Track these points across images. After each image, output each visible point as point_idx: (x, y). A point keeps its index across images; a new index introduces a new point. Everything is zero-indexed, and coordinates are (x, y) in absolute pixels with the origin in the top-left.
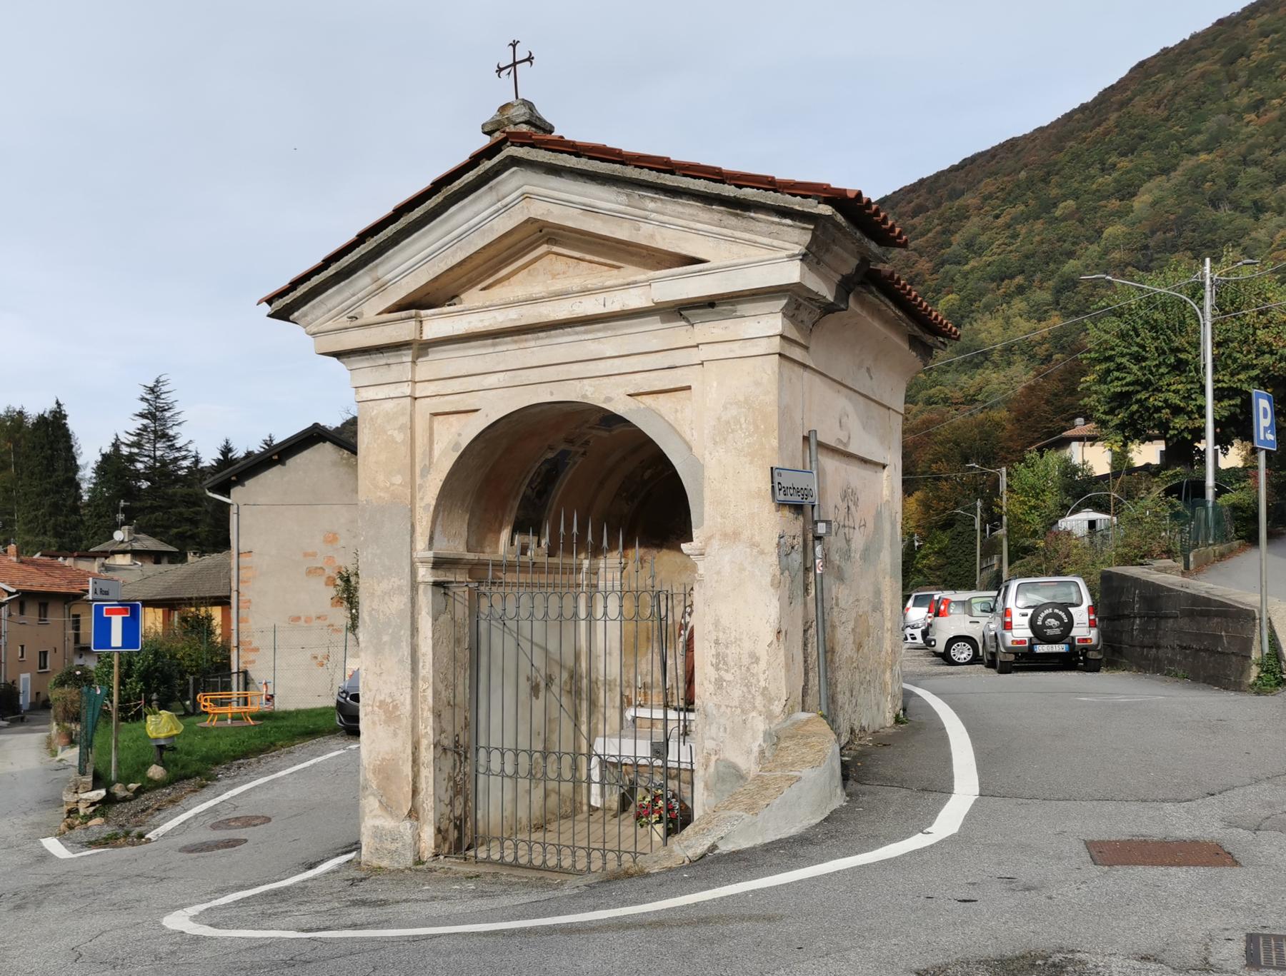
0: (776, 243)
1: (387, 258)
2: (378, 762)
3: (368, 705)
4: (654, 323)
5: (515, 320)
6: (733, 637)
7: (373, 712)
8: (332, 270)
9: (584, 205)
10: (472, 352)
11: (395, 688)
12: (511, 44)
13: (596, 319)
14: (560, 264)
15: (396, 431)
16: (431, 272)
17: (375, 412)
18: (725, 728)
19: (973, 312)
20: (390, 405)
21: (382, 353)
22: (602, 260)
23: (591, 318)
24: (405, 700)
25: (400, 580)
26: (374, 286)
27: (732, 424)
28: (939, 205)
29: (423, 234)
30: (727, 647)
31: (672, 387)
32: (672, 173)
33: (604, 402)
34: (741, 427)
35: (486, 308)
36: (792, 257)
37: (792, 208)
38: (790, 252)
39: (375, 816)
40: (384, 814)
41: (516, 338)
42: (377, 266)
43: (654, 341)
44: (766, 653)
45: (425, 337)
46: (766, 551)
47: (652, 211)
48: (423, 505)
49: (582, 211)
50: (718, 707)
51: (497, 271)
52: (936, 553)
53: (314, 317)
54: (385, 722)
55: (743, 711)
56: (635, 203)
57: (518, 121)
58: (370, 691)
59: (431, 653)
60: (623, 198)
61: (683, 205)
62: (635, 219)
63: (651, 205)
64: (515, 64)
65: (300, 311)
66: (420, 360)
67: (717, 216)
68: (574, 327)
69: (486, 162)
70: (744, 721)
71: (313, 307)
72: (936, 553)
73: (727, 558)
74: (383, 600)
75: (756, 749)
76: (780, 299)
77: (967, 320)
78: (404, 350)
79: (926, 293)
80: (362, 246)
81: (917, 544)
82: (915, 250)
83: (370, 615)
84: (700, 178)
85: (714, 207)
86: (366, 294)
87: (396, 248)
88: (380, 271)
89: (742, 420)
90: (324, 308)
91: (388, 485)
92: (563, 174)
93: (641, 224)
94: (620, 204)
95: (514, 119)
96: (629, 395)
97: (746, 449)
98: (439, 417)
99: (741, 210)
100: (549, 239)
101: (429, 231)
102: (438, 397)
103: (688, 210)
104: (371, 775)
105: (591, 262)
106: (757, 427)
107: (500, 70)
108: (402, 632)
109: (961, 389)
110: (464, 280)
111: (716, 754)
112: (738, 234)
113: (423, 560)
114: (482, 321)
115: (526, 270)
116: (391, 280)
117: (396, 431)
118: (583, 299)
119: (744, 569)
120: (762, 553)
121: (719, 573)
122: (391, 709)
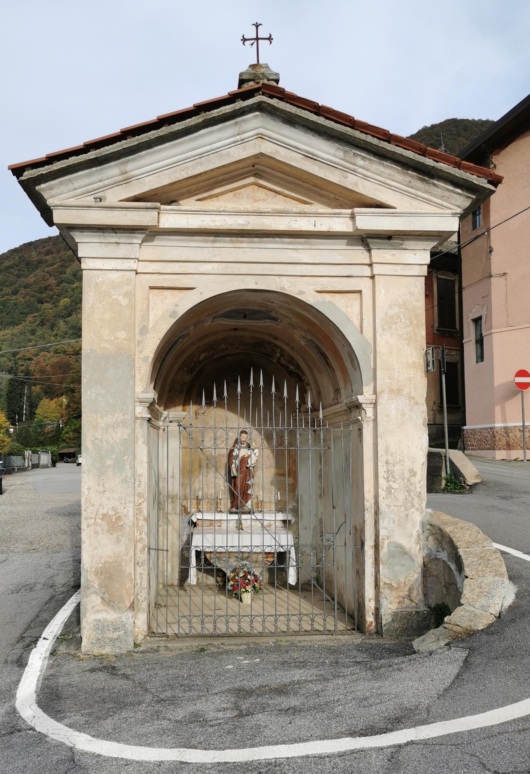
0: (445, 204)
1: (139, 157)
2: (101, 565)
3: (91, 518)
4: (341, 245)
5: (243, 225)
6: (398, 459)
7: (95, 524)
8: (92, 155)
9: (308, 152)
10: (193, 244)
11: (118, 503)
12: (254, 24)
13: (303, 235)
14: (261, 193)
15: (121, 297)
16: (172, 176)
17: (100, 279)
18: (394, 521)
19: (77, 309)
20: (115, 276)
21: (116, 233)
22: (293, 195)
23: (304, 233)
24: (128, 511)
25: (124, 415)
26: (121, 178)
27: (395, 318)
28: (59, 252)
29: (175, 145)
30: (394, 466)
31: (349, 289)
32: (389, 142)
33: (298, 294)
34: (401, 321)
35: (219, 212)
36: (454, 214)
37: (472, 182)
38: (454, 211)
39: (98, 611)
40: (106, 608)
41: (234, 239)
42: (128, 162)
43: (339, 257)
44: (420, 469)
45: (161, 226)
46: (419, 402)
47: (360, 167)
48: (141, 356)
49: (303, 157)
50: (389, 506)
51: (211, 189)
52: (73, 431)
53: (59, 192)
54: (108, 531)
55: (405, 509)
56: (348, 158)
57: (271, 78)
58: (93, 506)
59: (146, 474)
60: (340, 154)
61: (387, 166)
62: (345, 170)
63: (361, 162)
64: (257, 39)
65: (48, 184)
66: (144, 244)
67: (408, 179)
68: (282, 238)
69: (241, 102)
70: (407, 515)
71: (61, 183)
72: (73, 431)
73: (393, 406)
74: (107, 431)
75: (415, 534)
76: (434, 242)
77: (74, 312)
78: (138, 233)
79: (53, 296)
80: (123, 142)
81: (61, 426)
82: (47, 272)
83: (93, 442)
84: (409, 150)
85: (409, 172)
86: (112, 182)
87: (148, 151)
88: (130, 166)
89: (402, 316)
90: (71, 186)
91: (113, 338)
92: (296, 126)
93: (349, 174)
94: (337, 157)
95: (267, 76)
96: (316, 291)
97: (405, 335)
98: (154, 290)
99: (428, 177)
100: (256, 174)
101: (179, 144)
102: (157, 275)
103: (388, 171)
104: (93, 577)
105: (286, 196)
106: (411, 322)
107: (244, 40)
108: (126, 458)
109: (72, 347)
110: (185, 190)
111: (388, 539)
112: (420, 193)
113: (141, 400)
114: (214, 221)
115: (232, 193)
116: (136, 176)
117: (121, 297)
118: (298, 219)
119: (405, 414)
120: (417, 403)
121: (388, 416)
122: (113, 520)
